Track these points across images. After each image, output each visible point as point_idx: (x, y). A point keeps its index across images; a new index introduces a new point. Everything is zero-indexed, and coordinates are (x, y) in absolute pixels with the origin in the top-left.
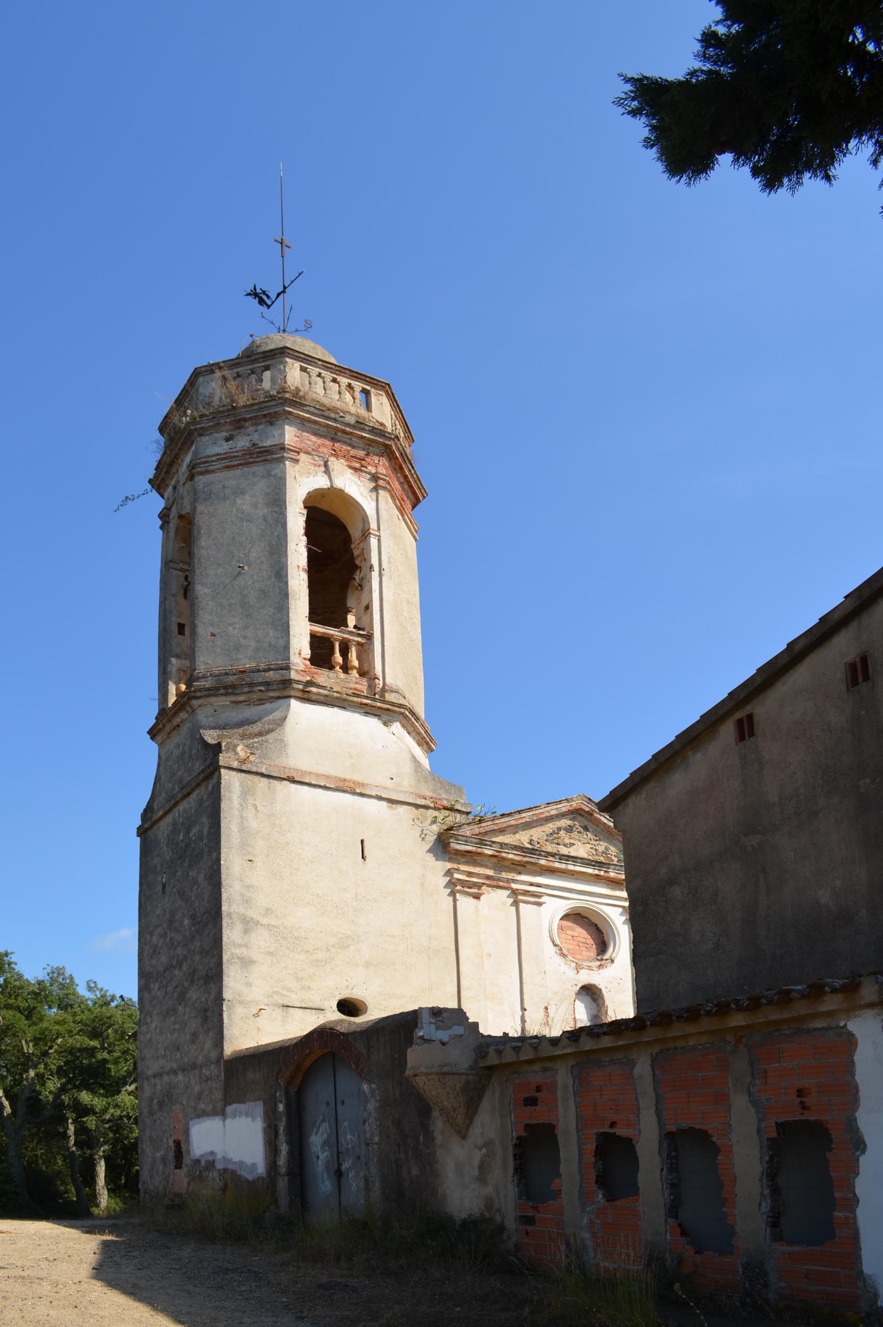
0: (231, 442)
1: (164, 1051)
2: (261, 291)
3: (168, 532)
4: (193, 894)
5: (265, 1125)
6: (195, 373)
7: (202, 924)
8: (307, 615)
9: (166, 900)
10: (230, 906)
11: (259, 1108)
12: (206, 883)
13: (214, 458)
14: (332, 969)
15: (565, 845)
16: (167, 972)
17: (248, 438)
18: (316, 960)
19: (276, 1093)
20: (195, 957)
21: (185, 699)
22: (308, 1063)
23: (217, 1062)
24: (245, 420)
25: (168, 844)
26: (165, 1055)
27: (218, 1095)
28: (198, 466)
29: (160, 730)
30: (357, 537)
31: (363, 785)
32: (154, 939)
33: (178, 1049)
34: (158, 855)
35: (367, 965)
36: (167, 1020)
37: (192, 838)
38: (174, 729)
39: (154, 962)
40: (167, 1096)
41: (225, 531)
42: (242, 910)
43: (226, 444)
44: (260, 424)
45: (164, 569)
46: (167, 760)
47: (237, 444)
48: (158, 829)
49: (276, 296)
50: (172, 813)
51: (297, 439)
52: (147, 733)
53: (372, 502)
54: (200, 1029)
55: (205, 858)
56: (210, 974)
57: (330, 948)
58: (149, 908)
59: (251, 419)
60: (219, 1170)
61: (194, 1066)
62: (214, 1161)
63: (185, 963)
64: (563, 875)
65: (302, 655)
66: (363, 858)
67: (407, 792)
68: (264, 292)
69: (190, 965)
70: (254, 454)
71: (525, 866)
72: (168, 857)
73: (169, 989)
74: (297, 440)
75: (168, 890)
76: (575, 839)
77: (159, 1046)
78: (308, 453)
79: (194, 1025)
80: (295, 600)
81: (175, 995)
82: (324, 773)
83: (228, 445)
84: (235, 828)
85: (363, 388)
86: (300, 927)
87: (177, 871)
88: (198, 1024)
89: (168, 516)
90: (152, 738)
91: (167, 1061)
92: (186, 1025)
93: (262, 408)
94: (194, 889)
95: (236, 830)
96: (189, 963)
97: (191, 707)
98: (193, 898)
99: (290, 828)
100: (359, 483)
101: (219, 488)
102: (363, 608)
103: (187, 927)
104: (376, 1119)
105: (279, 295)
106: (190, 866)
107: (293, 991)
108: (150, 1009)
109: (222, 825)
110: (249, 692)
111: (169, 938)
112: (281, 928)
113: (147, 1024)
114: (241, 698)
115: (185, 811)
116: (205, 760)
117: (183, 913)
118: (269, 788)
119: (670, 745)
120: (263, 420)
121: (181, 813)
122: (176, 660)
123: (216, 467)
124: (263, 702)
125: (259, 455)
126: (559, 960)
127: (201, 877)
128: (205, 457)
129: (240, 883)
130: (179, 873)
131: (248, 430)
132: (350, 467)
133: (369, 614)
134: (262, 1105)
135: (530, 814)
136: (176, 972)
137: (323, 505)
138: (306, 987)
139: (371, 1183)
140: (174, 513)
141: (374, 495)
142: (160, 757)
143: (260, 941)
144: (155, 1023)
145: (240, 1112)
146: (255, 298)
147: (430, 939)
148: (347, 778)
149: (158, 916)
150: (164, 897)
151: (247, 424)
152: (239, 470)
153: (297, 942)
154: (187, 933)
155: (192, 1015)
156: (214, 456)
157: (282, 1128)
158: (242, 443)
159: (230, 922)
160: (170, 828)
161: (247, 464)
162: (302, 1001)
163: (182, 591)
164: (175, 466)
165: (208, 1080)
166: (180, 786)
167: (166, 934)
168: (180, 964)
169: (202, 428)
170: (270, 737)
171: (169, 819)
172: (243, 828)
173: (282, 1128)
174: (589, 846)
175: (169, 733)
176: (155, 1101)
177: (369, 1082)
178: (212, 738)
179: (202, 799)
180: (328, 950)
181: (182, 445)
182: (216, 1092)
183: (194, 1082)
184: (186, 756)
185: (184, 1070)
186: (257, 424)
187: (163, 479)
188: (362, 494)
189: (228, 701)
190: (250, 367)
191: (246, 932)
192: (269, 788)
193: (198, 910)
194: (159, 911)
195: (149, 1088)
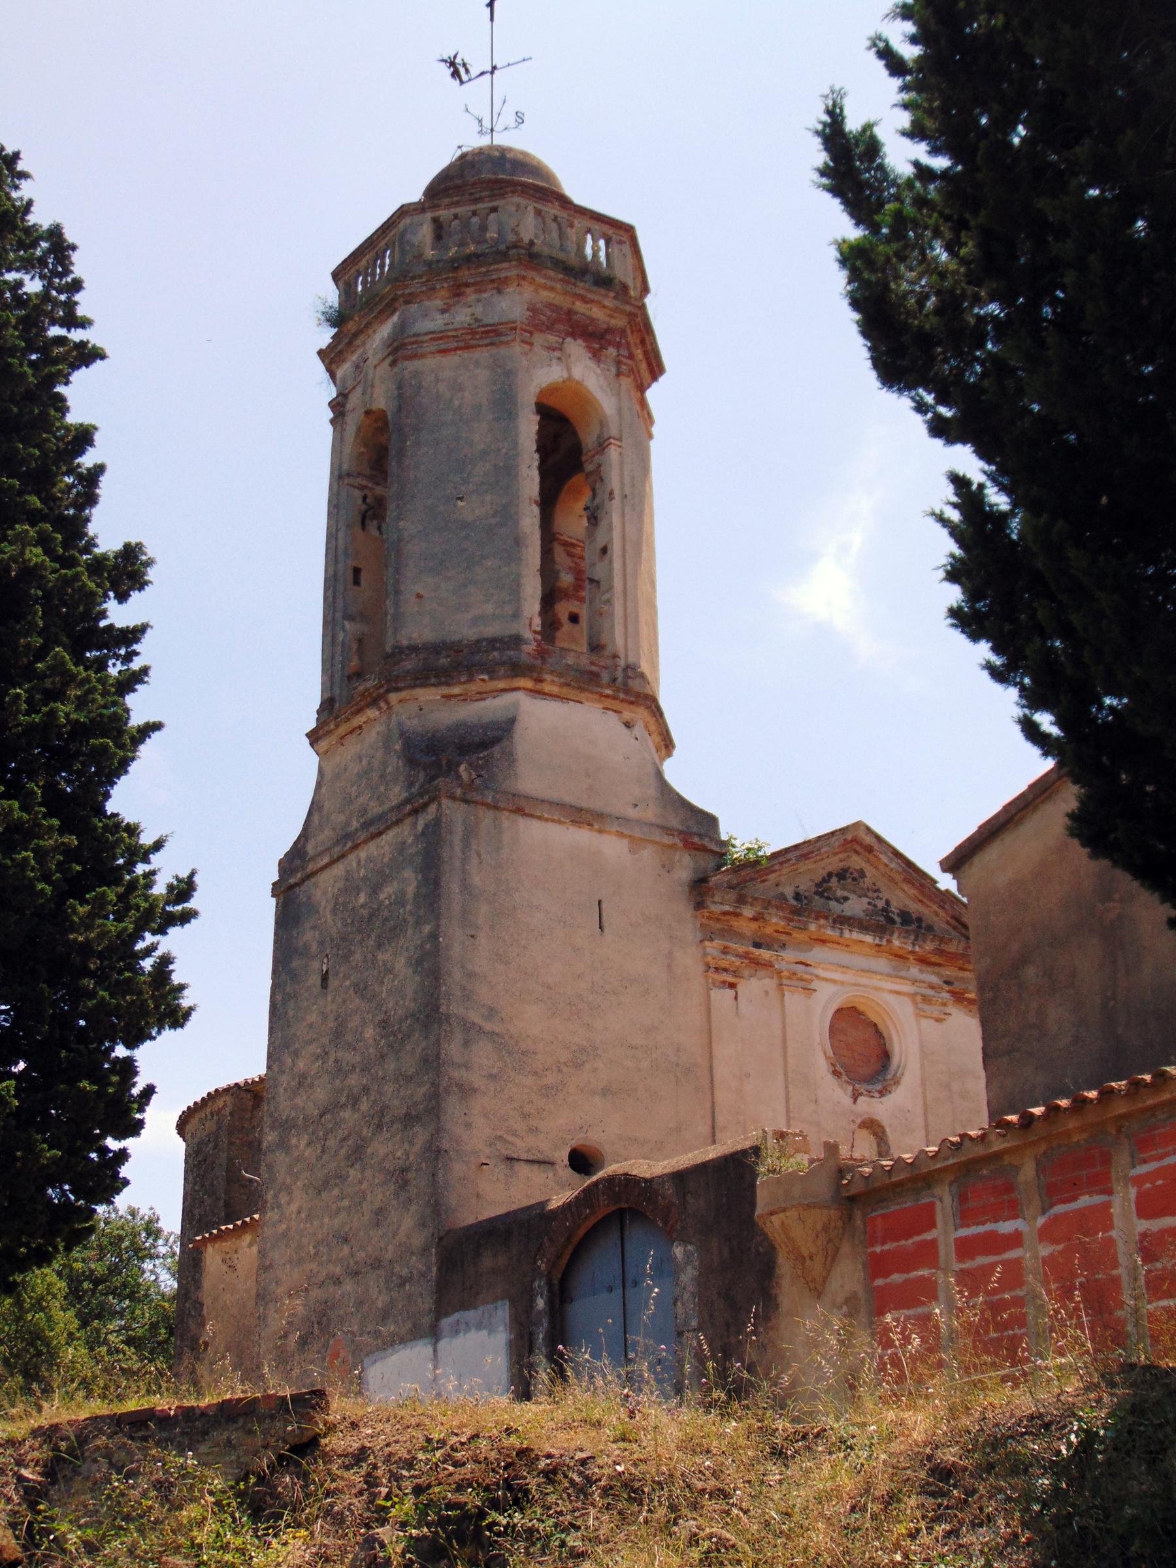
0: (447, 315)
1: (315, 1247)
3: (343, 430)
4: (384, 988)
5: (513, 1337)
7: (400, 1036)
9: (329, 998)
10: (448, 1006)
11: (502, 1312)
12: (410, 970)
15: (837, 900)
16: (328, 1116)
17: (469, 310)
18: (546, 1087)
19: (533, 1281)
20: (386, 1088)
21: (381, 691)
22: (581, 1232)
23: (425, 1250)
24: (467, 285)
25: (334, 911)
26: (316, 1254)
27: (426, 1303)
29: (330, 732)
30: (590, 446)
32: (301, 1064)
34: (314, 928)
35: (605, 1092)
36: (324, 1195)
37: (383, 902)
38: (351, 732)
39: (299, 1101)
40: (318, 1323)
42: (461, 1011)
44: (485, 291)
45: (335, 484)
46: (337, 776)
48: (316, 885)
50: (345, 861)
52: (307, 735)
55: (409, 933)
58: (291, 1013)
59: (474, 284)
61: (376, 1264)
64: (836, 946)
67: (652, 824)
68: (464, 65)
69: (375, 1101)
70: (477, 333)
71: (790, 934)
72: (334, 931)
73: (332, 1143)
75: (333, 983)
76: (850, 891)
77: (305, 1241)
79: (380, 1196)
81: (343, 1152)
84: (455, 887)
87: (352, 953)
89: (343, 406)
90: (312, 744)
91: (320, 1264)
92: (364, 1197)
94: (386, 981)
96: (372, 1098)
97: (388, 703)
98: (384, 995)
100: (598, 371)
102: (598, 551)
103: (371, 1041)
104: (693, 1295)
105: (482, 74)
106: (379, 946)
108: (289, 1180)
111: (332, 1060)
113: (279, 1206)
114: (456, 690)
115: (370, 860)
116: (411, 784)
117: (364, 1019)
119: (1022, 796)
120: (490, 286)
121: (363, 862)
123: (428, 350)
127: (401, 962)
128: (415, 335)
130: (358, 956)
133: (606, 561)
134: (507, 1307)
136: (346, 1114)
137: (551, 402)
140: (354, 400)
142: (321, 772)
143: (483, 1055)
145: (467, 1324)
149: (311, 1026)
150: (326, 994)
151: (468, 290)
154: (371, 1050)
156: (426, 334)
157: (541, 1336)
158: (462, 316)
160: (340, 885)
161: (467, 347)
162: (529, 1150)
163: (359, 519)
164: (362, 337)
165: (405, 1282)
166: (362, 821)
167: (326, 1054)
168: (355, 1101)
169: (410, 294)
170: (496, 749)
171: (339, 869)
172: (466, 887)
174: (865, 900)
175: (342, 738)
177: (685, 1241)
179: (404, 843)
180: (560, 1071)
181: (380, 313)
182: (420, 1300)
183: (377, 1289)
184: (375, 775)
186: (480, 291)
187: (341, 352)
188: (601, 387)
190: (473, 207)
194: (313, 1017)
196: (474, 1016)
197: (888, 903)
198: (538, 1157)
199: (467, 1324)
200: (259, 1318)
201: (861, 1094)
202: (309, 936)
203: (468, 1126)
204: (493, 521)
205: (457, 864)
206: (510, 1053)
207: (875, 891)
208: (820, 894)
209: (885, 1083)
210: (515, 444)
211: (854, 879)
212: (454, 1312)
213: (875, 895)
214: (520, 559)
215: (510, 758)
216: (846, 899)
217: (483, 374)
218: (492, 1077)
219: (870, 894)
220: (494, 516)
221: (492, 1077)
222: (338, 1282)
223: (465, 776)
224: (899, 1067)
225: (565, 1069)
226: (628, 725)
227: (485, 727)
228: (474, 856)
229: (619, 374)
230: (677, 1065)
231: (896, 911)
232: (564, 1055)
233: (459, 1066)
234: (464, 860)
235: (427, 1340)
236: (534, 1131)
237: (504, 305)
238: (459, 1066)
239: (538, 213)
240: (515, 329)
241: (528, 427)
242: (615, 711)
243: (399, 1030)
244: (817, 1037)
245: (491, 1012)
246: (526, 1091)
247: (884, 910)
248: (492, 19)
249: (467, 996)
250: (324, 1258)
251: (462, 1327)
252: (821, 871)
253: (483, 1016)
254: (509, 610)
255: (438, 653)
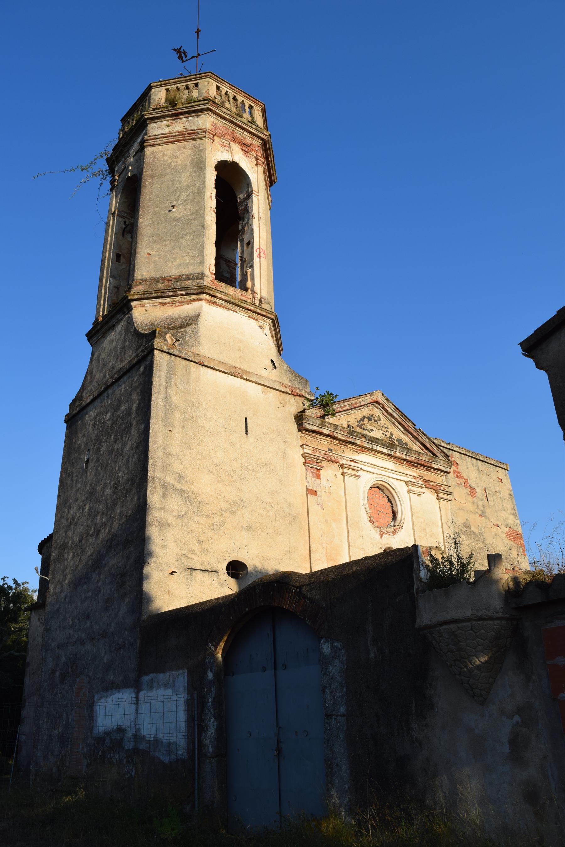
1: (72, 620)
2: (183, 51)
4: (117, 465)
6: (150, 87)
8: (215, 243)
10: (154, 472)
13: (159, 136)
14: (224, 532)
15: (368, 430)
17: (182, 125)
18: (214, 524)
26: (73, 624)
28: (147, 141)
31: (247, 372)
33: (88, 617)
35: (249, 529)
40: (72, 667)
41: (162, 183)
43: (167, 128)
47: (174, 128)
49: (191, 57)
51: (213, 127)
53: (254, 174)
54: (116, 595)
56: (130, 539)
57: (223, 512)
60: (128, 750)
62: (122, 740)
63: (103, 530)
65: (211, 270)
66: (246, 433)
68: (185, 53)
74: (213, 128)
78: (218, 136)
80: (208, 230)
82: (223, 361)
83: (169, 129)
85: (250, 105)
86: (203, 493)
88: (113, 589)
90: (89, 340)
92: (100, 591)
93: (194, 106)
95: (162, 404)
99: (199, 405)
100: (247, 161)
101: (160, 156)
105: (193, 57)
107: (196, 554)
109: (153, 399)
110: (173, 296)
112: (190, 494)
114: (167, 300)
118: (186, 370)
122: (113, 280)
124: (182, 304)
125: (189, 135)
126: (369, 524)
129: (162, 451)
131: (182, 120)
132: (242, 149)
134: (186, 674)
135: (349, 403)
138: (206, 550)
139: (335, 766)
141: (256, 167)
144: (65, 593)
145: (158, 683)
146: (177, 54)
147: (290, 506)
148: (237, 367)
152: (175, 145)
153: (201, 506)
155: (107, 581)
156: (159, 135)
157: (210, 700)
159: (153, 486)
162: (202, 564)
170: (188, 329)
173: (210, 700)
176: (58, 674)
178: (145, 330)
180: (222, 515)
185: (92, 639)
188: (248, 168)
189: (157, 303)
191: (164, 495)
192: (186, 370)
193: (121, 479)
195: (51, 659)
196: (170, 479)
197: (391, 434)
198: (208, 567)
199: (158, 683)
200: (42, 659)
201: (384, 533)
202: (81, 440)
203: (164, 547)
204: (191, 217)
205: (163, 388)
206: (192, 503)
207: (386, 428)
208: (360, 427)
209: (395, 528)
210: (204, 182)
211: (375, 421)
212: (150, 673)
213: (386, 430)
214: (204, 235)
215: (196, 334)
216: (372, 430)
217: (188, 152)
218: (181, 517)
219: (383, 429)
220: (191, 215)
221: (181, 517)
222: (83, 643)
223: (169, 340)
224: (401, 519)
225: (225, 514)
226: (261, 327)
227: (182, 319)
228: (173, 385)
229: (257, 165)
230: (289, 514)
231: (396, 439)
232: (225, 506)
233: (159, 509)
234: (167, 386)
235: (132, 690)
236: (205, 551)
237: (200, 122)
238: (159, 509)
239: (218, 88)
240: (205, 132)
241: (211, 176)
242: (255, 319)
243: (124, 489)
244: (361, 502)
245: (181, 477)
246: (201, 526)
247: (390, 438)
248: (198, 38)
249: (165, 467)
250: (77, 627)
251: (155, 684)
252: (360, 415)
253: (175, 479)
254: (198, 260)
255: (157, 282)
